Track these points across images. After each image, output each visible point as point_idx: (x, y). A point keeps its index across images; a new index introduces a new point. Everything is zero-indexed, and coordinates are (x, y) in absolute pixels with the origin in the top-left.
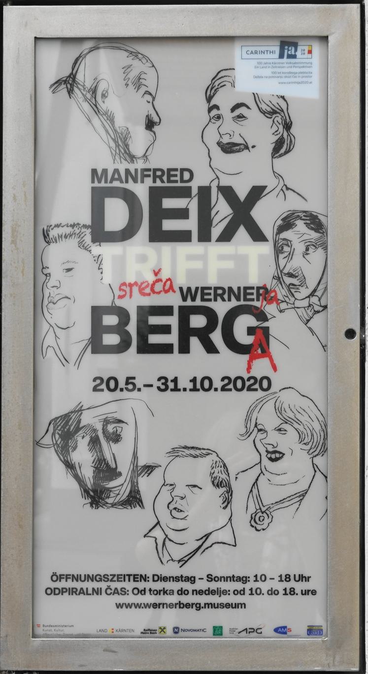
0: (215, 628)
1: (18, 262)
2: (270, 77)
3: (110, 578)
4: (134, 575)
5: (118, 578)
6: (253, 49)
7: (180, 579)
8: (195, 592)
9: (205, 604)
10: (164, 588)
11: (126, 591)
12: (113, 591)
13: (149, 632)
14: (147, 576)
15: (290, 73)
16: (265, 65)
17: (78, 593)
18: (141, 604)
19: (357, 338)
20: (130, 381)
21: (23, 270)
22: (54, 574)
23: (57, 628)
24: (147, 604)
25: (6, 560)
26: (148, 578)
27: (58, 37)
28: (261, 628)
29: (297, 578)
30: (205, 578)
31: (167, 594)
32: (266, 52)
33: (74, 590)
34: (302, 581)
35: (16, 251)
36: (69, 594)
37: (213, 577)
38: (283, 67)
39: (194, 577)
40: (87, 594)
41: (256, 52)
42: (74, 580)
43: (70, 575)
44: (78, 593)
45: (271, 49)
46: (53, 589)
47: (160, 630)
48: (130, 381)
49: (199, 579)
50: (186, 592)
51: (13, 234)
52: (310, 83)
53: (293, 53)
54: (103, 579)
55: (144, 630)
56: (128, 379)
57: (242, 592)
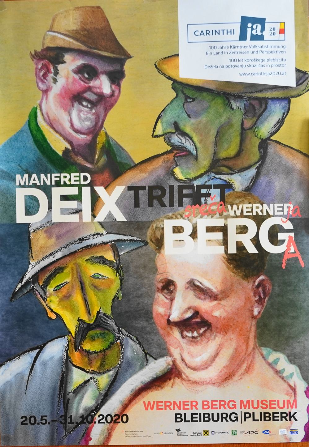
0: (232, 431)
13: (197, 434)
16: (220, 51)
20: (43, 418)
41: (208, 33)
48: (43, 418)
52: (284, 74)
53: (259, 33)
56: (42, 417)
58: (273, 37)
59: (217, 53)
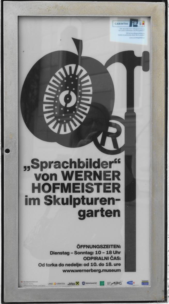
0: (101, 282)
3: (103, 246)
4: (114, 245)
5: (107, 247)
7: (63, 253)
8: (67, 265)
9: (103, 270)
10: (53, 263)
11: (119, 258)
12: (113, 258)
13: (72, 284)
14: (120, 246)
16: (123, 30)
17: (98, 259)
18: (74, 270)
22: (78, 245)
23: (30, 283)
24: (77, 270)
26: (120, 246)
28: (121, 282)
29: (115, 253)
30: (70, 253)
31: (54, 266)
33: (97, 258)
34: (117, 254)
36: (94, 260)
37: (77, 252)
39: (69, 252)
40: (102, 260)
42: (118, 246)
43: (85, 245)
44: (98, 259)
46: (87, 258)
47: (76, 283)
49: (71, 253)
50: (63, 265)
53: (136, 24)
54: (100, 247)
55: (69, 283)
57: (88, 265)
58: (141, 26)
59: (122, 31)
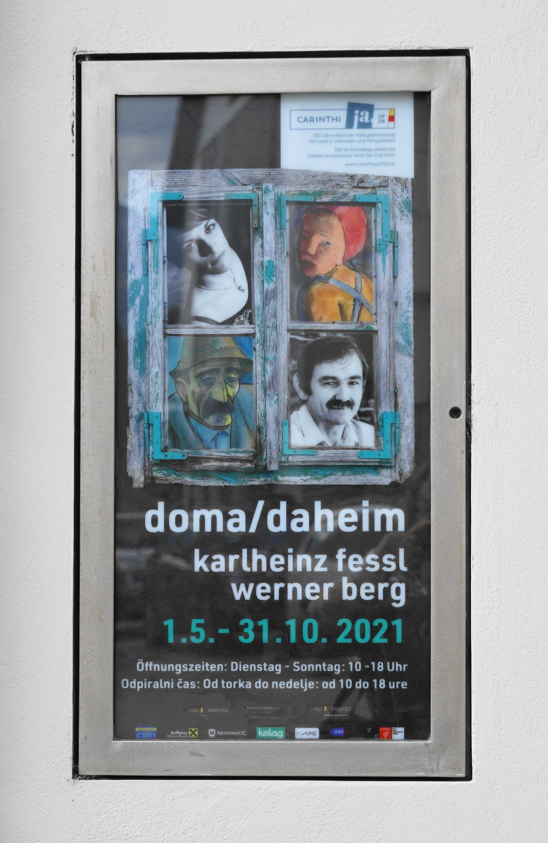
1: (98, 337)
2: (332, 156)
6: (308, 114)
15: (363, 150)
16: (325, 139)
19: (463, 416)
21: (103, 345)
25: (85, 656)
27: (141, 94)
32: (326, 119)
35: (96, 325)
38: (351, 141)
41: (312, 119)
45: (334, 114)
51: (92, 306)
53: (367, 120)
